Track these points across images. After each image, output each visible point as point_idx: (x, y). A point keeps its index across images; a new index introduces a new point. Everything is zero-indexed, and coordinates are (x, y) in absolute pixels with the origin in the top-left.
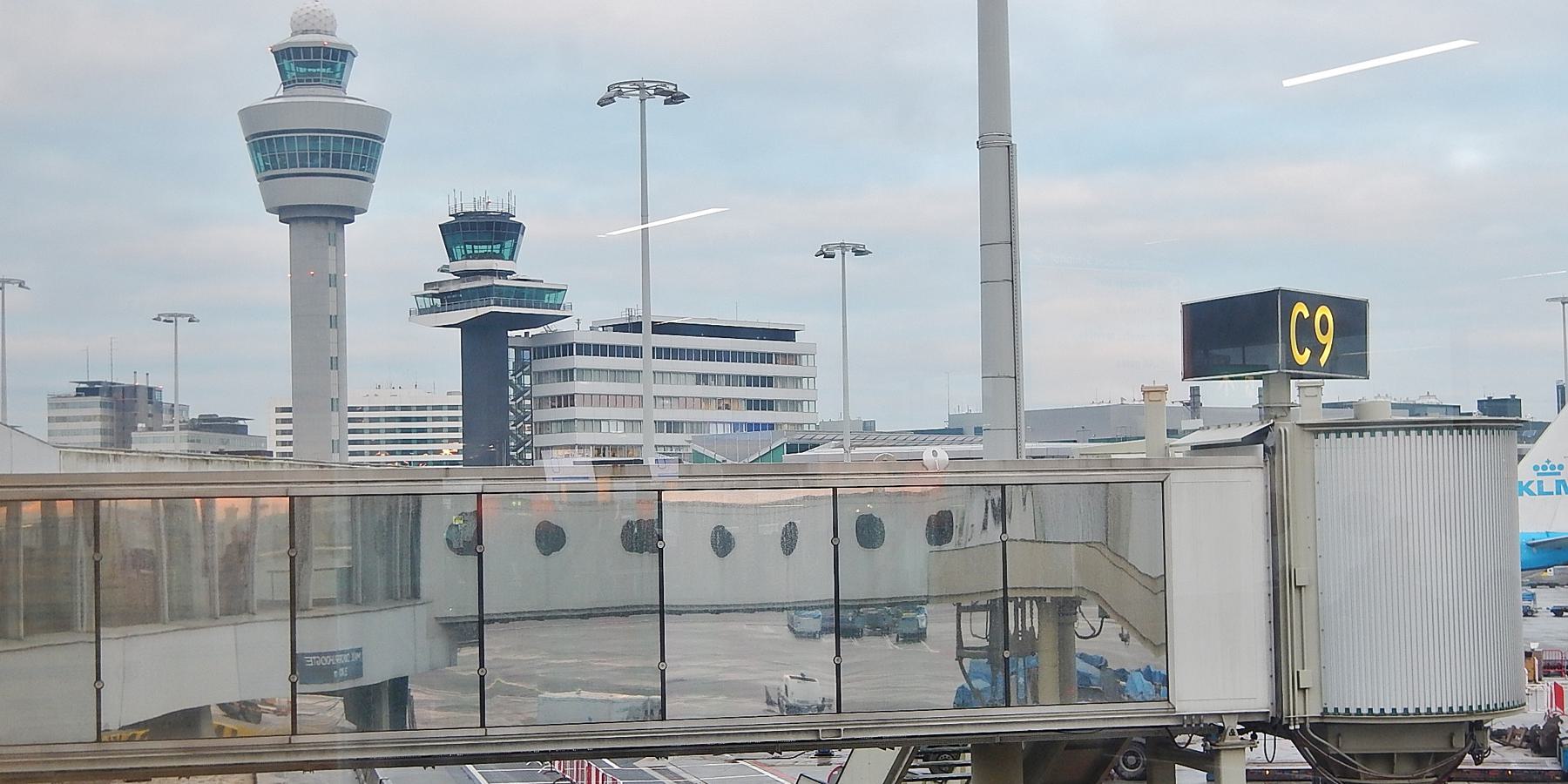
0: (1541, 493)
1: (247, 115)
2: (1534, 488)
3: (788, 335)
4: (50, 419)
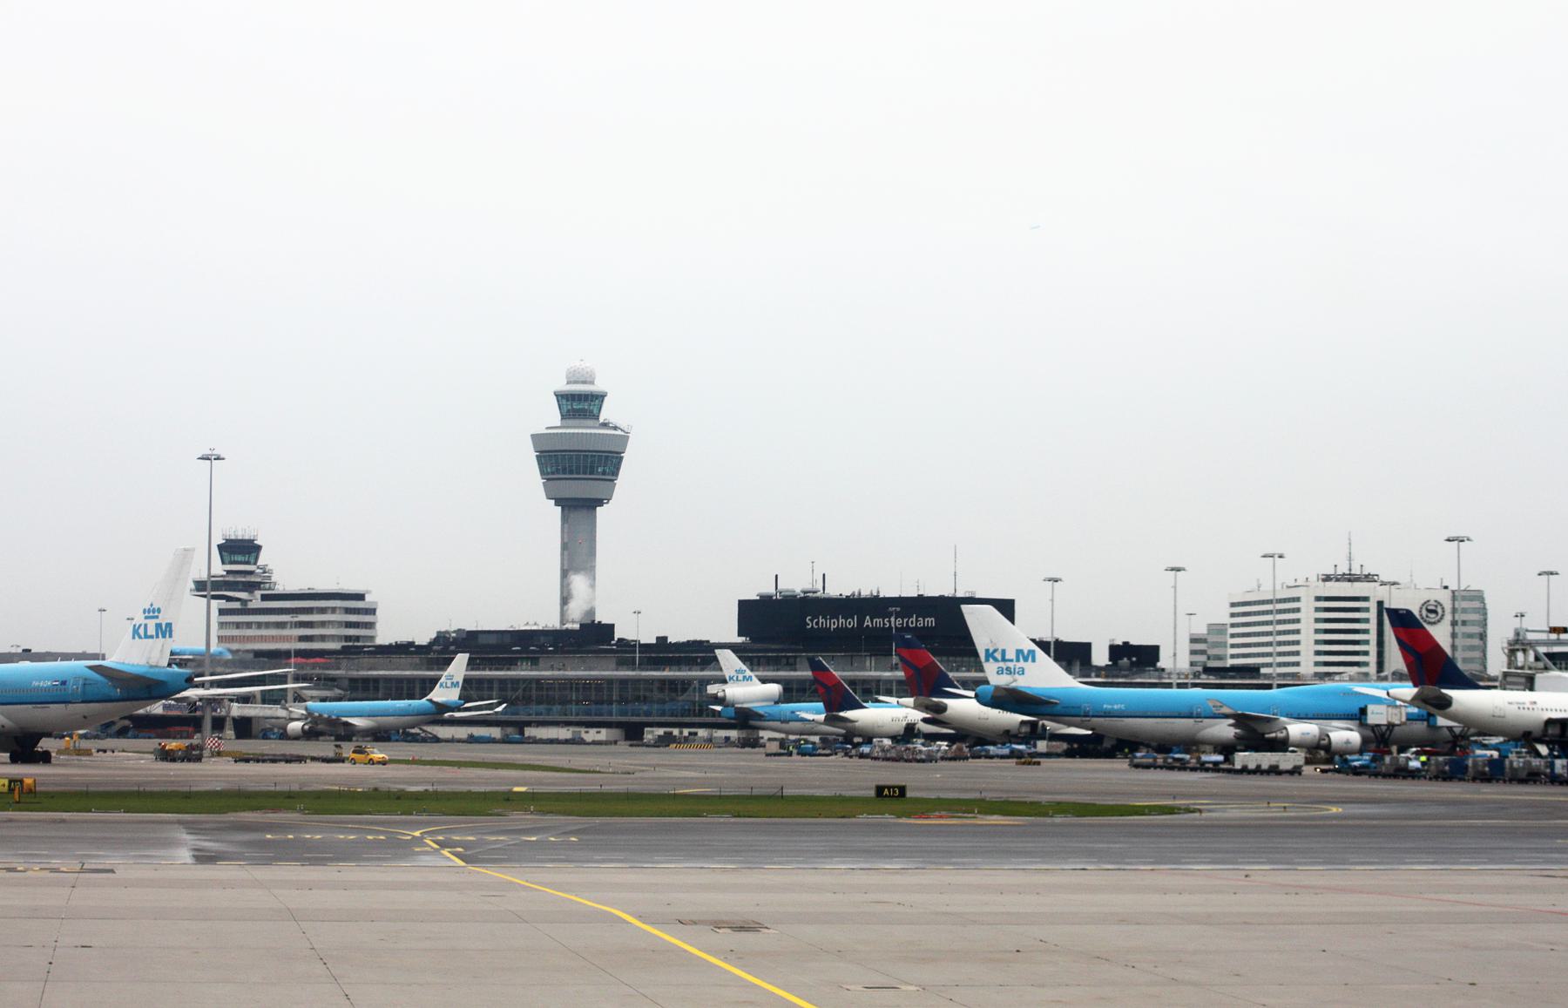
0: (147, 636)
1: (536, 438)
2: (141, 631)
3: (360, 597)
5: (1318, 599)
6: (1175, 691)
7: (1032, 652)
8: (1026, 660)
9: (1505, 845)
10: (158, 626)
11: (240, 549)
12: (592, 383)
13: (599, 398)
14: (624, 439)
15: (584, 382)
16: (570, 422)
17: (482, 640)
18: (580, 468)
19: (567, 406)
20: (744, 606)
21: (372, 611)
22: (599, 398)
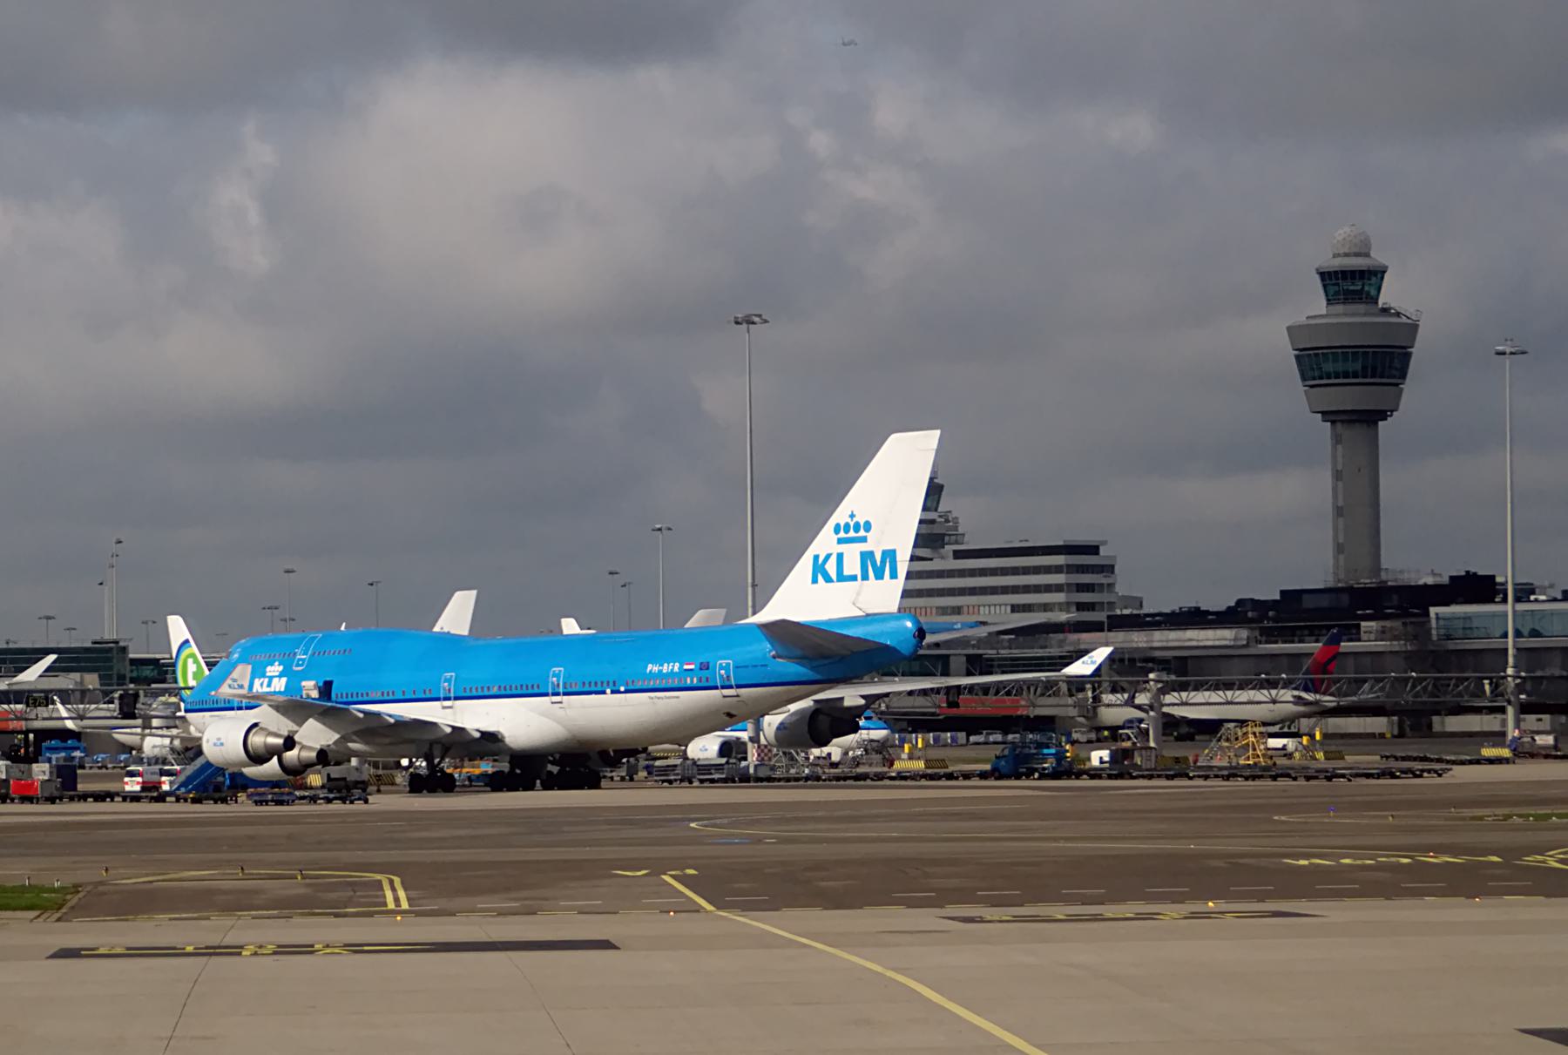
0: (842, 577)
2: (831, 567)
6: (90, 806)
10: (867, 557)
12: (1367, 255)
13: (1378, 274)
14: (1413, 328)
16: (1340, 308)
17: (1308, 603)
21: (1109, 569)
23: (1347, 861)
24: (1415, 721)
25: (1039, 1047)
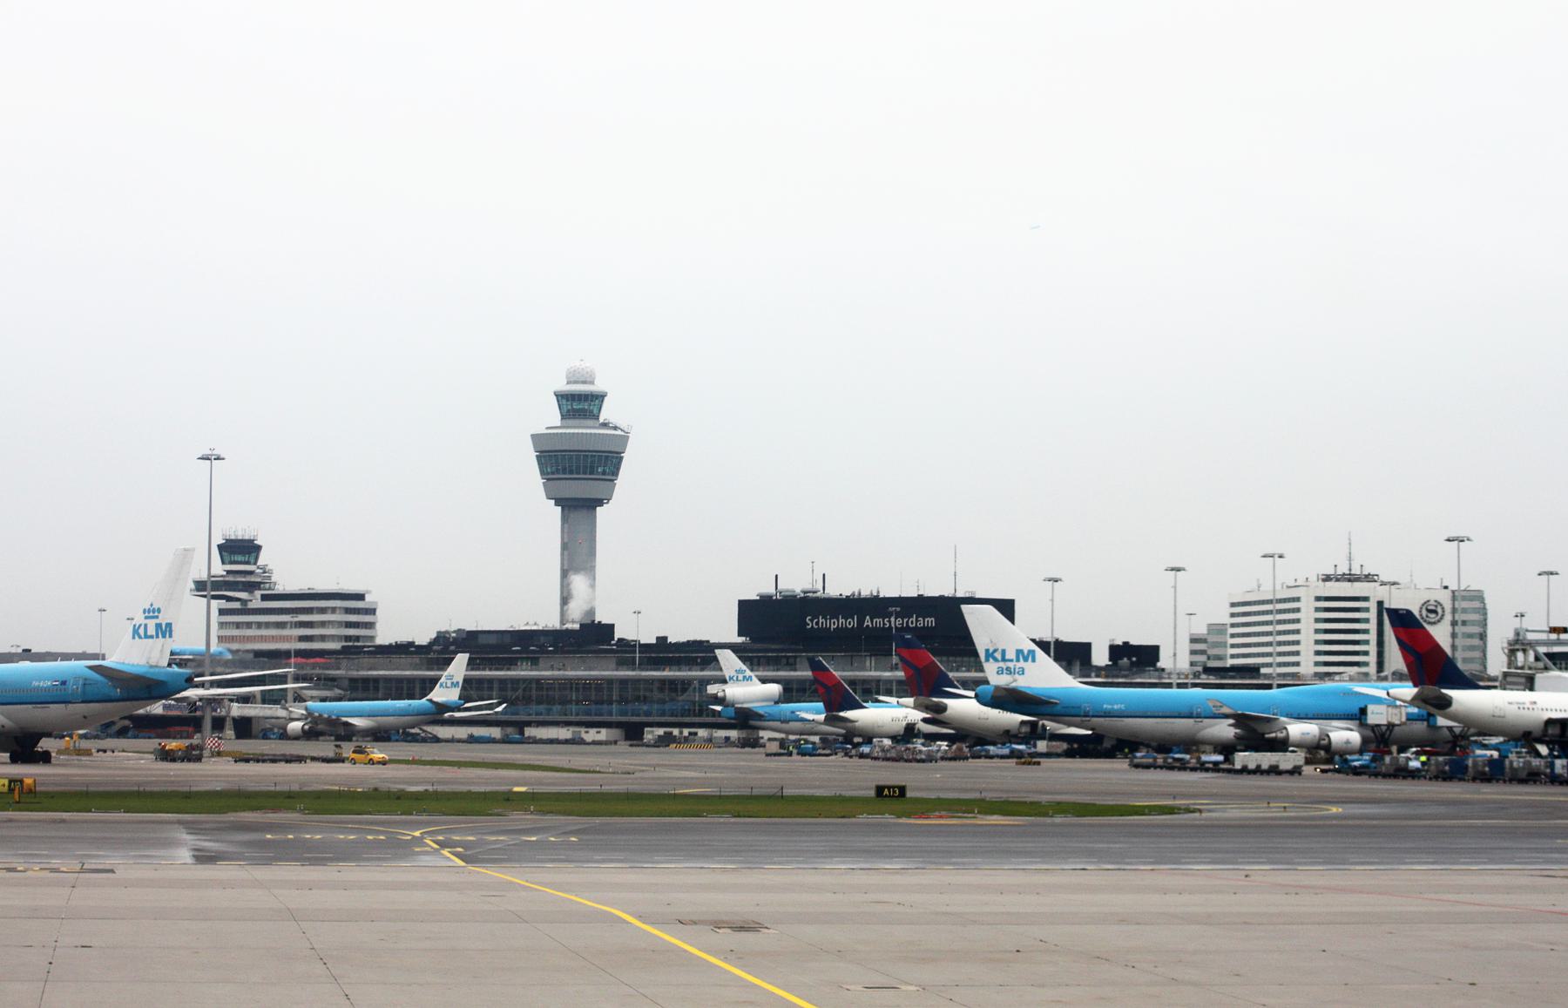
0: (147, 636)
1: (536, 438)
2: (141, 631)
3: (360, 597)
4: (1193, 652)
5: (1318, 599)
6: (1175, 691)
7: (1032, 652)
8: (1026, 660)
9: (1505, 845)
10: (158, 626)
11: (240, 549)
12: (592, 383)
13: (599, 398)
14: (624, 439)
15: (584, 382)
16: (570, 422)
17: (482, 640)
18: (580, 468)
19: (567, 406)
20: (744, 606)
21: (372, 611)
22: (599, 398)
23: (1334, 810)
24: (1517, 634)
25: (809, 1002)
